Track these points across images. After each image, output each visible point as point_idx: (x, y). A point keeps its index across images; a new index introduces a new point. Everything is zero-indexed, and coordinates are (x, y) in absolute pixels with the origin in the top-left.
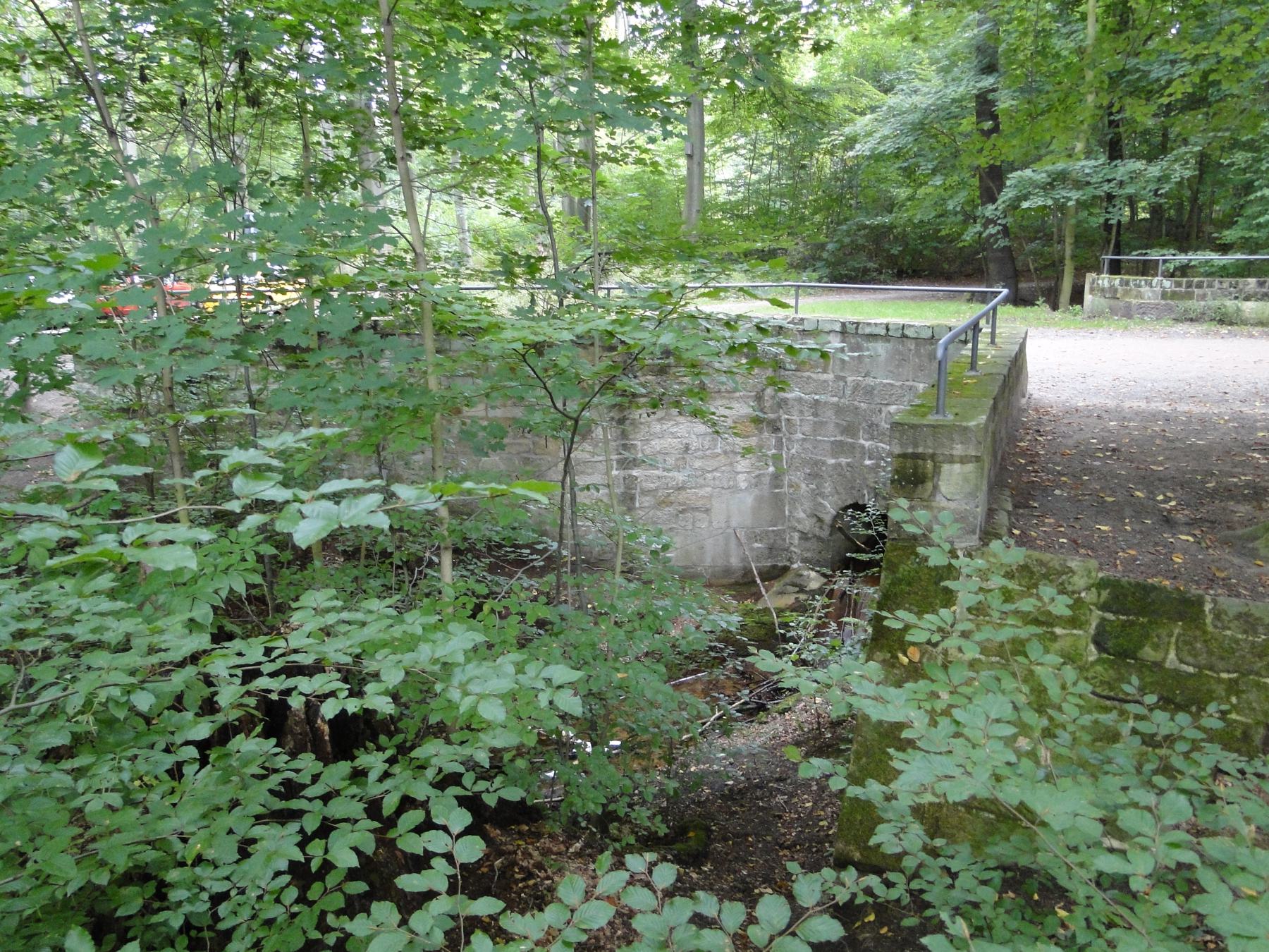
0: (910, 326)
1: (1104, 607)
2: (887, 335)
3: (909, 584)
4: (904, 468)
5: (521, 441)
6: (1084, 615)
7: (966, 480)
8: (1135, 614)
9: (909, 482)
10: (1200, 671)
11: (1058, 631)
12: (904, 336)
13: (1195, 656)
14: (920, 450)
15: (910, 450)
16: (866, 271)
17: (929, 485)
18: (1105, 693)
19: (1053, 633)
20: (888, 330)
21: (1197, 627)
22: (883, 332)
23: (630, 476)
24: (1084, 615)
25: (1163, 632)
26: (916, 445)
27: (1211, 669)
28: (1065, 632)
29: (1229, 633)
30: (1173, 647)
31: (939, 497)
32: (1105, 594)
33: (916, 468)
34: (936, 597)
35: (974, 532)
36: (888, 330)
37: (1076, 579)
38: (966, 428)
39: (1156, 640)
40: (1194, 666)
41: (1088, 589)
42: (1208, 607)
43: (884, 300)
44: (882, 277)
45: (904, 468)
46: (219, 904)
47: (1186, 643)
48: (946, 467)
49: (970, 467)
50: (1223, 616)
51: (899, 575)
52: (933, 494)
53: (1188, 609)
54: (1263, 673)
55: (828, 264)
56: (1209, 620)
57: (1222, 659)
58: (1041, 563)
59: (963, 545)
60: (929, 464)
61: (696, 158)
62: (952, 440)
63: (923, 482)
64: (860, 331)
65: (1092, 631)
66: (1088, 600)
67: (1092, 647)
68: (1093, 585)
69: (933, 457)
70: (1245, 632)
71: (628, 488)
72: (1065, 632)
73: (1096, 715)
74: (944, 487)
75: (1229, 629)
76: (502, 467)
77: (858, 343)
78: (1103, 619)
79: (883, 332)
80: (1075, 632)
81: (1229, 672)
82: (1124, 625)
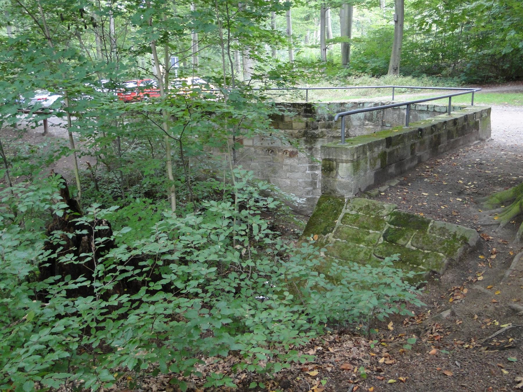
0: (437, 106)
1: (391, 223)
2: (427, 110)
3: (323, 211)
4: (326, 164)
5: (268, 157)
6: (382, 225)
7: (348, 170)
8: (402, 226)
9: (328, 170)
10: (418, 249)
11: (371, 231)
12: (434, 111)
13: (417, 244)
14: (331, 157)
15: (327, 157)
16: (489, 77)
17: (335, 172)
18: (379, 256)
19: (368, 232)
20: (428, 108)
21: (423, 232)
22: (426, 109)
23: (314, 173)
24: (382, 225)
25: (409, 234)
26: (329, 156)
27: (422, 248)
28: (373, 232)
29: (434, 235)
30: (411, 239)
31: (338, 177)
32: (393, 218)
33: (330, 165)
34: (331, 216)
35: (351, 191)
36: (428, 108)
37: (384, 211)
38: (347, 149)
39: (406, 236)
40: (416, 247)
41: (387, 215)
42: (431, 224)
43: (503, 92)
44: (498, 81)
45: (326, 164)
46: (99, 321)
47: (416, 238)
48: (340, 164)
49: (349, 165)
50: (434, 228)
51: (321, 208)
52: (336, 175)
53: (422, 225)
54: (439, 251)
55: (466, 74)
56: (428, 230)
57: (427, 244)
58: (374, 205)
59: (348, 197)
60: (335, 163)
61: (399, 23)
62: (342, 153)
63: (332, 170)
64: (417, 109)
65: (384, 232)
66: (386, 220)
67: (382, 238)
68: (389, 214)
69: (336, 160)
70: (440, 235)
71: (313, 179)
72: (373, 232)
73: (298, 249)
74: (340, 173)
75: (435, 233)
76: (259, 168)
77: (416, 114)
78: (390, 227)
79: (426, 109)
80: (377, 232)
81: (428, 250)
82: (396, 230)
